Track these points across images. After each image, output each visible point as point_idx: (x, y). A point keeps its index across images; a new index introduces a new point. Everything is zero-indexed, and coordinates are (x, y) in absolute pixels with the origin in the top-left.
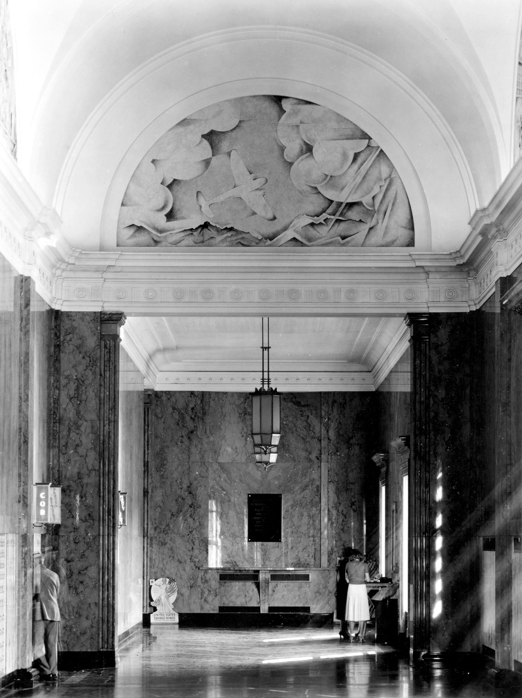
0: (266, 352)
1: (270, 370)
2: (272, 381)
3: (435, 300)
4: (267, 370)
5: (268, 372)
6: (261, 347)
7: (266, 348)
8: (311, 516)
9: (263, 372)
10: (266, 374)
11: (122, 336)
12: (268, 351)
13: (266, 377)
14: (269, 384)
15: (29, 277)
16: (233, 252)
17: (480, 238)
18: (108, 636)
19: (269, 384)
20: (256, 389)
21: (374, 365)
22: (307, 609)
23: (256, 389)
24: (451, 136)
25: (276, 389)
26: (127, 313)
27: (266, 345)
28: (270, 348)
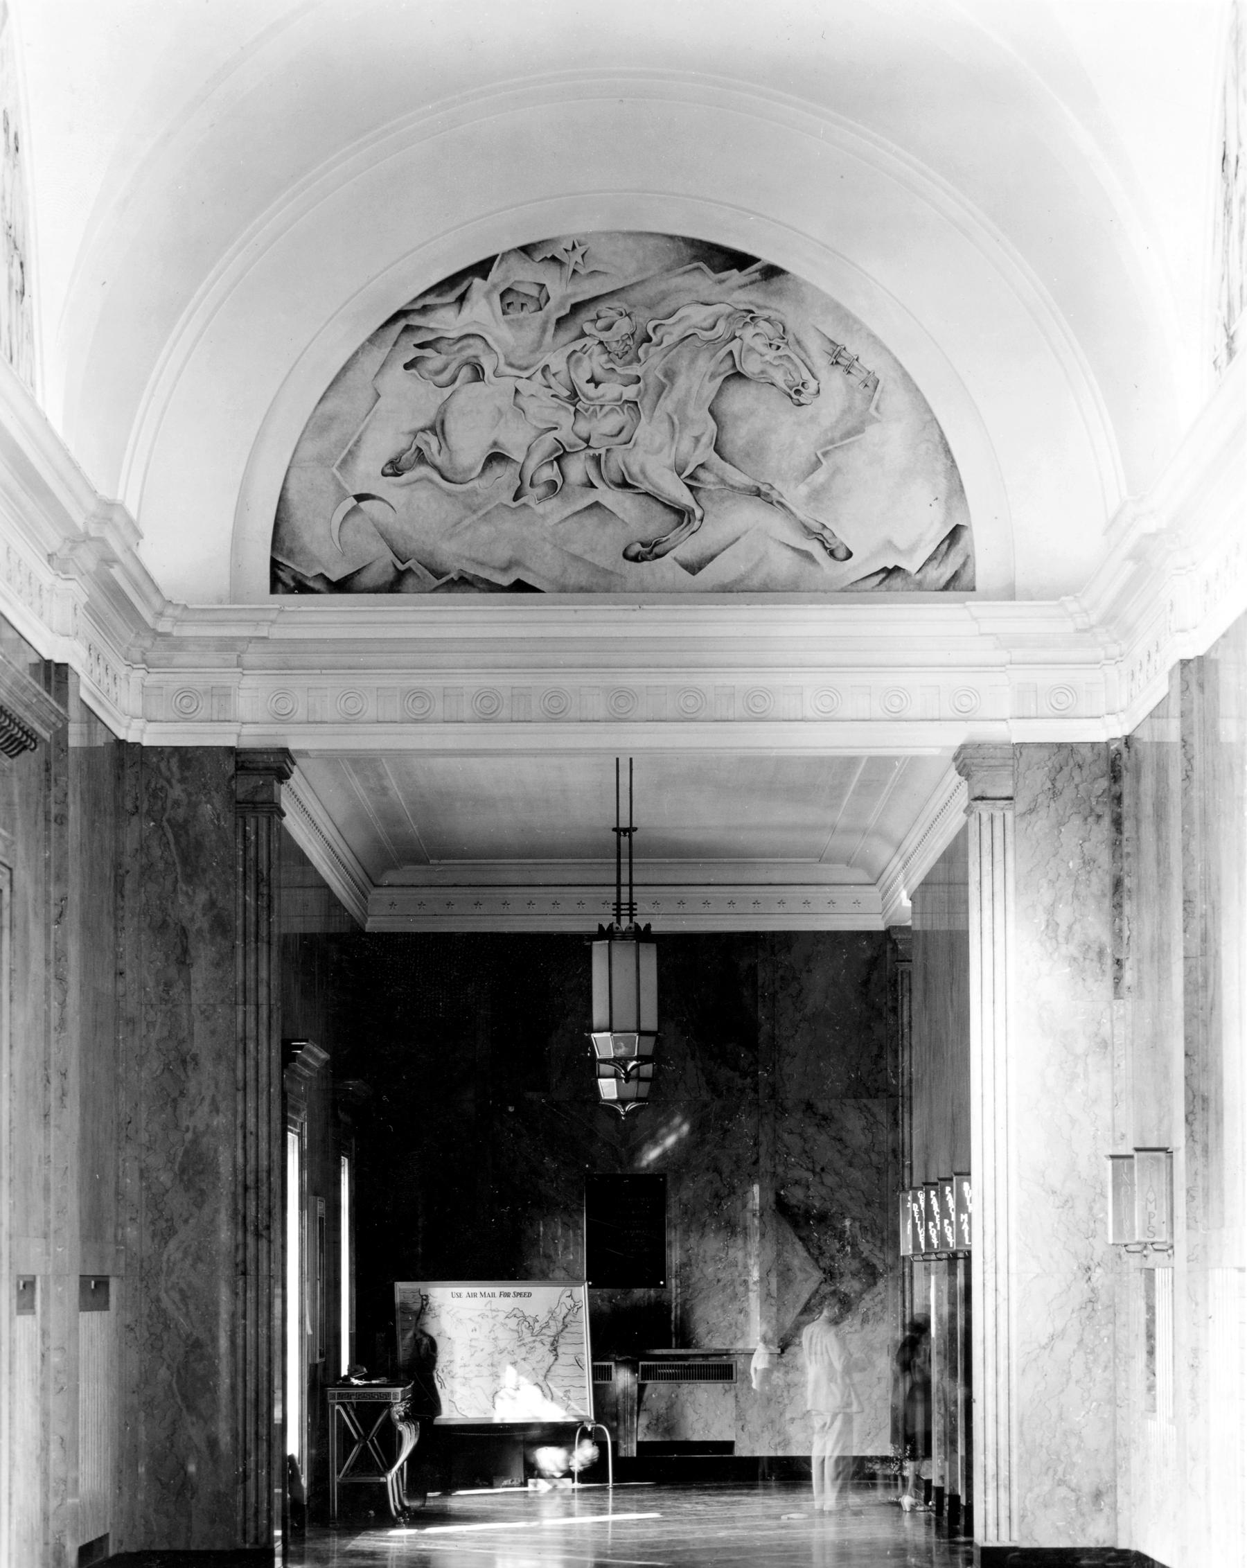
0: (625, 840)
1: (635, 881)
2: (641, 907)
3: (215, 718)
4: (627, 882)
5: (631, 885)
6: (614, 830)
7: (625, 830)
8: (1111, 1310)
9: (619, 885)
10: (625, 890)
11: (286, 803)
12: (630, 837)
13: (625, 898)
14: (631, 915)
15: (66, 665)
16: (561, 603)
17: (1130, 566)
18: (257, 1496)
19: (631, 915)
20: (601, 926)
21: (880, 870)
22: (729, 1446)
23: (601, 926)
24: (132, 461)
25: (648, 926)
26: (297, 751)
27: (624, 824)
28: (635, 829)
